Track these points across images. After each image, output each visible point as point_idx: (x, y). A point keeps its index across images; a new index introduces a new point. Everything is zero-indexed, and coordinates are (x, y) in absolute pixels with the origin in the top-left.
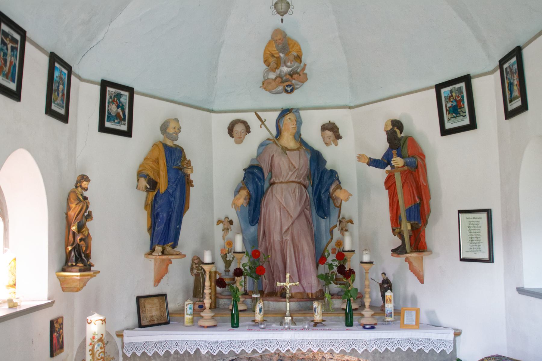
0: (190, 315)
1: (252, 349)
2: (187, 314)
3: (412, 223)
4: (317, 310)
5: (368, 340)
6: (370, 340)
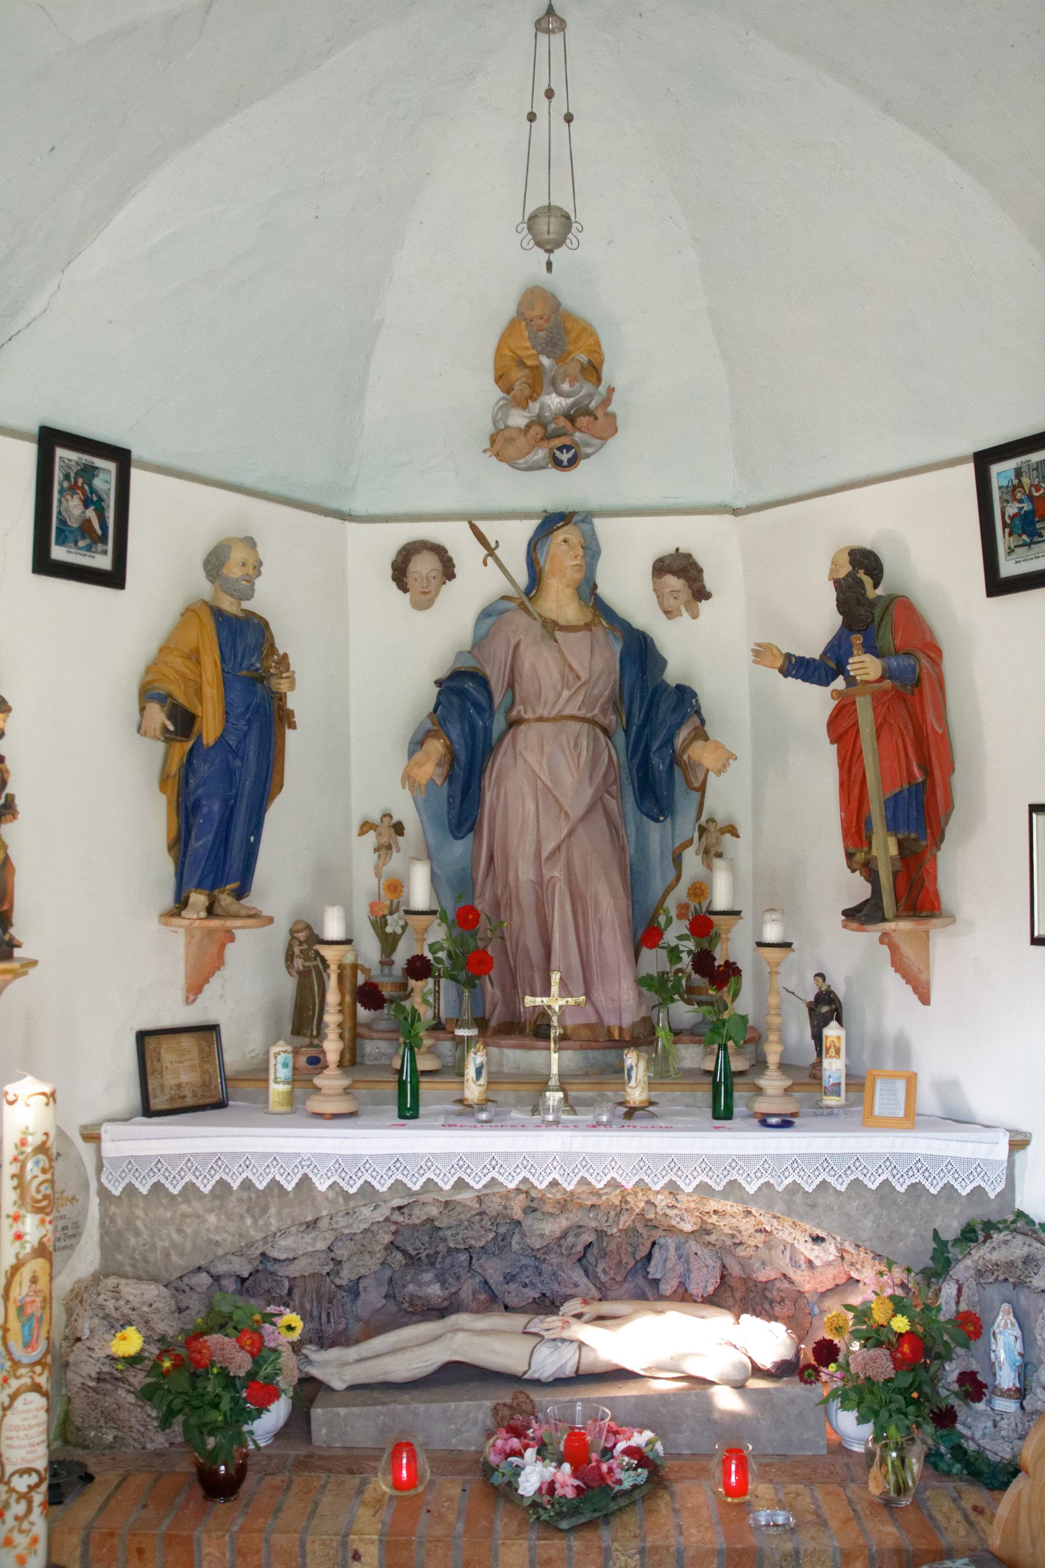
0: (285, 1082)
2: (276, 1081)
4: (633, 1074)
6: (779, 1158)
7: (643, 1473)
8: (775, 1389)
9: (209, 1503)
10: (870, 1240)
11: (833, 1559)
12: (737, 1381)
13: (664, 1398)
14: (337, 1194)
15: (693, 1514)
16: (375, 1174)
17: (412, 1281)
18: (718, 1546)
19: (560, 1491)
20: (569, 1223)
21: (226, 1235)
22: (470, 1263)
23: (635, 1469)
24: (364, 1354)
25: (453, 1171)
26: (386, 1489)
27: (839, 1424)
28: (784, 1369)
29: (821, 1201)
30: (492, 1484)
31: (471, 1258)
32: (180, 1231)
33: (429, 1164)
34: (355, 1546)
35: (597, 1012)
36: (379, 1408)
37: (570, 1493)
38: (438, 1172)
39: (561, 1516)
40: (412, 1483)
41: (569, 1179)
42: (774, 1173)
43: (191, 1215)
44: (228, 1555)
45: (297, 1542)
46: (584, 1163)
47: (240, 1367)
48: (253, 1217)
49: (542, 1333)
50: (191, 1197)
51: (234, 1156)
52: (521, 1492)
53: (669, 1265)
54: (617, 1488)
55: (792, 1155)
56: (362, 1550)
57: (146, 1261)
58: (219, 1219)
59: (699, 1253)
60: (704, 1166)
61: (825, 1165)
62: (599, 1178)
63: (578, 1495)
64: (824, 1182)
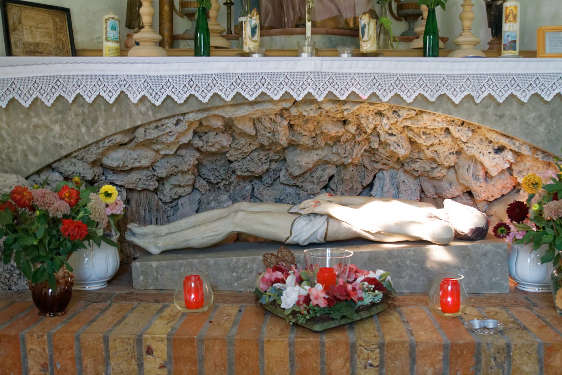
0: (114, 41)
1: (234, 93)
2: (107, 40)
3: (316, 281)
4: (366, 30)
5: (474, 76)
6: (479, 77)
7: (379, 295)
8: (472, 246)
9: (41, 317)
10: (543, 142)
11: (538, 351)
12: (445, 239)
13: (390, 253)
14: (148, 109)
15: (417, 325)
16: (174, 90)
17: (214, 200)
18: (444, 342)
19: (314, 302)
20: (318, 158)
21: (68, 140)
22: (253, 192)
23: (374, 291)
24: (173, 230)
25: (232, 87)
26: (181, 309)
27: (519, 272)
28: (479, 234)
29: (507, 113)
30: (261, 304)
31: (253, 188)
32: (34, 138)
33: (215, 82)
34: (148, 343)
35: (339, 10)
36: (181, 261)
37: (322, 304)
38: (221, 88)
39: (314, 320)
40: (199, 303)
41: (320, 92)
42: (474, 88)
43: (42, 126)
44: (47, 350)
45: (102, 340)
46: (331, 81)
47: (58, 210)
48: (87, 126)
49: (300, 212)
50: (40, 112)
51: (70, 78)
52: (283, 306)
53: (385, 189)
54: (359, 303)
55: (488, 75)
56: (154, 347)
57: (10, 160)
58: (62, 129)
59: (406, 181)
60: (421, 82)
61: (513, 82)
62: (342, 92)
63: (328, 305)
64: (512, 96)
